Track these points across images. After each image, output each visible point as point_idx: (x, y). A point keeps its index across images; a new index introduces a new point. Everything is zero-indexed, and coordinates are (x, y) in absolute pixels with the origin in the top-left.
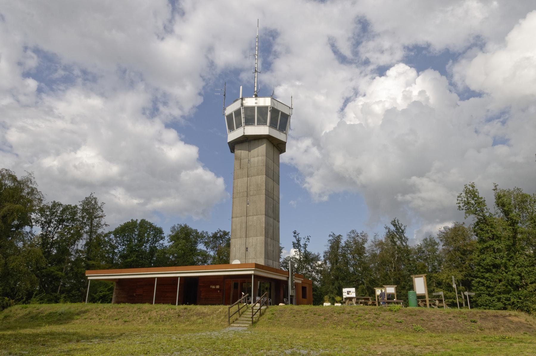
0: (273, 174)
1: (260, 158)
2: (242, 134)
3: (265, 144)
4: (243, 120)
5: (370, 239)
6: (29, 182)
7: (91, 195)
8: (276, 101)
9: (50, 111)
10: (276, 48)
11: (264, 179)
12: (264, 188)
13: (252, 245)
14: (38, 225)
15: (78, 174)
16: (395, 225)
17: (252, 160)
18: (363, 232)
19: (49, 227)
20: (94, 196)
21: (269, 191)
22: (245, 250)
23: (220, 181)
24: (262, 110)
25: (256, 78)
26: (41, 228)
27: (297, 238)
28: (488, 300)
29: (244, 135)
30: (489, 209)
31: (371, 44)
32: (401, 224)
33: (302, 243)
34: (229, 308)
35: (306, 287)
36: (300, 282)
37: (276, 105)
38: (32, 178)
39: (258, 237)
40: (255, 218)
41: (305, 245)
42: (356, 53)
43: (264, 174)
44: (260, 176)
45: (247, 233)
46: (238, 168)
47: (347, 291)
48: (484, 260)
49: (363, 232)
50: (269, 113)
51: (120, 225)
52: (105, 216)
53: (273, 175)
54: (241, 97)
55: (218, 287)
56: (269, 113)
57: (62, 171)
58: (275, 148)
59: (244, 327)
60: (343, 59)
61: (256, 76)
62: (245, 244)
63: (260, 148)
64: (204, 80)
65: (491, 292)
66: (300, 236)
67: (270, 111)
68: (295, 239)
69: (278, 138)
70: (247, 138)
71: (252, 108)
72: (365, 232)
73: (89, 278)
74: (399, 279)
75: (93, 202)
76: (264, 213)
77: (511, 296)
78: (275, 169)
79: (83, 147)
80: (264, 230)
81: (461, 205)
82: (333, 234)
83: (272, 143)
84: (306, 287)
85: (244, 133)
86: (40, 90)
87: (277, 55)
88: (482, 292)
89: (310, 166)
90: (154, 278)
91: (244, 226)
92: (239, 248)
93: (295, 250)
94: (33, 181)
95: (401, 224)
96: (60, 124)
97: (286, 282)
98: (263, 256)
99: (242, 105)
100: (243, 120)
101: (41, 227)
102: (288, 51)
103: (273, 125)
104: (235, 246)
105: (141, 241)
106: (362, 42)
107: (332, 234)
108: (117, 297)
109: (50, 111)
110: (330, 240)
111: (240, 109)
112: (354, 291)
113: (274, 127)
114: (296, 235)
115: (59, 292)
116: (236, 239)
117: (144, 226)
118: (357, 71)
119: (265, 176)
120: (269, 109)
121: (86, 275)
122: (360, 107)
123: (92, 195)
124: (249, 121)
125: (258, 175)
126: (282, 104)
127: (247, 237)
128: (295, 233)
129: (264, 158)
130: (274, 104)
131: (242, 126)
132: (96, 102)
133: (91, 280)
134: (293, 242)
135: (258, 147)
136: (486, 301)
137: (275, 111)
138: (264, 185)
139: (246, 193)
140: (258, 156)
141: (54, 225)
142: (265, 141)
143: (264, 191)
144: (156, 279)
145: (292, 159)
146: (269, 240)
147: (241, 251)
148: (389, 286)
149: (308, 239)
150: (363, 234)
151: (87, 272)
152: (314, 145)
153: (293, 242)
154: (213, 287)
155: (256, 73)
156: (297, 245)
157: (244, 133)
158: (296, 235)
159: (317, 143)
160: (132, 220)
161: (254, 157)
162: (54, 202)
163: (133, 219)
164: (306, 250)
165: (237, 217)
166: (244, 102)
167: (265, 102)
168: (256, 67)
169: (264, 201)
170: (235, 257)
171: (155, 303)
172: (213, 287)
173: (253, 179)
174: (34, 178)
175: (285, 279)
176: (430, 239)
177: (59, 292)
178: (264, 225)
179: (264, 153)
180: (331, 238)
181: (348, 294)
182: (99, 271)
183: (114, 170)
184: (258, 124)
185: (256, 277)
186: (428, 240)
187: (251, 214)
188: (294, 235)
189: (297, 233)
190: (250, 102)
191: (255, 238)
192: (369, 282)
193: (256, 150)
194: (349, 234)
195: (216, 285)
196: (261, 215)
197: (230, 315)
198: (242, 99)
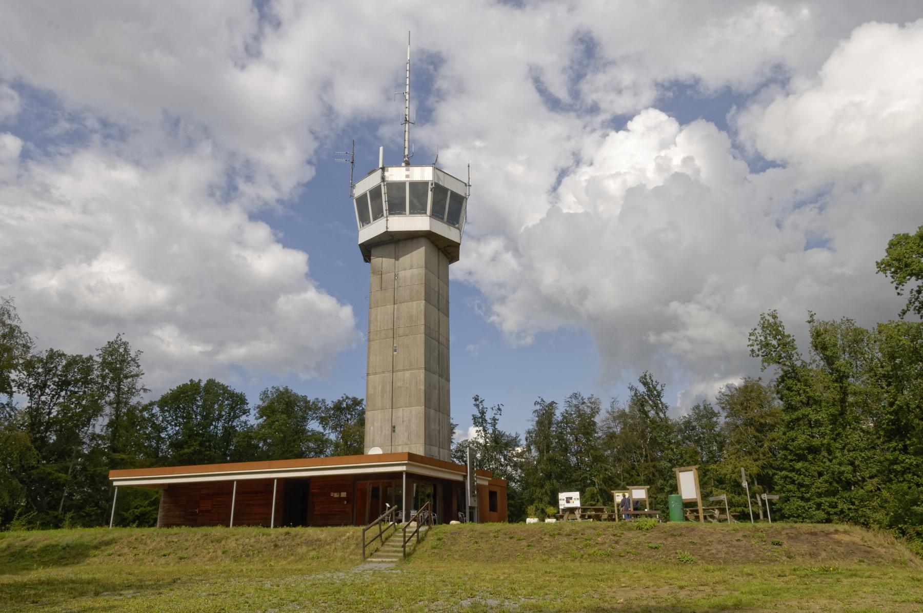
1: (415, 271)
3: (424, 247)
4: (385, 206)
6: (6, 316)
7: (117, 337)
8: (443, 173)
9: (44, 193)
11: (423, 307)
12: (423, 322)
13: (403, 421)
14: (22, 391)
15: (95, 301)
16: (645, 384)
17: (402, 274)
19: (42, 395)
20: (123, 340)
21: (432, 327)
22: (390, 431)
23: (347, 312)
24: (418, 188)
26: (29, 397)
28: (800, 506)
29: (387, 232)
30: (801, 354)
31: (601, 79)
32: (656, 382)
33: (488, 416)
34: (364, 531)
35: (496, 492)
36: (486, 483)
37: (442, 180)
38: (11, 309)
39: (413, 408)
40: (407, 374)
41: (494, 419)
42: (575, 94)
44: (414, 302)
45: (394, 400)
48: (793, 441)
50: (430, 194)
51: (170, 390)
52: (143, 374)
53: (438, 301)
54: (381, 166)
55: (344, 495)
56: (430, 194)
57: (66, 296)
58: (441, 253)
59: (389, 562)
60: (554, 104)
61: (407, 129)
63: (414, 253)
64: (316, 138)
65: (805, 493)
67: (431, 190)
69: (447, 237)
70: (392, 236)
71: (400, 186)
72: (595, 396)
73: (115, 484)
74: (654, 475)
75: (121, 350)
76: (423, 366)
77: (837, 499)
79: (103, 255)
80: (423, 395)
81: (756, 348)
82: (542, 400)
83: (437, 246)
84: (496, 492)
86: (25, 155)
87: (441, 96)
88: (791, 494)
89: (502, 285)
90: (232, 482)
92: (381, 427)
94: (13, 313)
95: (656, 382)
96: (62, 215)
97: (462, 485)
98: (422, 441)
99: (383, 179)
101: (28, 396)
102: (461, 89)
103: (437, 214)
105: (208, 419)
106: (585, 75)
107: (539, 400)
108: (165, 516)
109: (44, 193)
110: (536, 411)
112: (578, 497)
113: (438, 217)
117: (213, 390)
118: (579, 123)
120: (430, 186)
121: (110, 479)
122: (584, 184)
123: (119, 338)
124: (396, 208)
125: (412, 300)
126: (449, 177)
127: (394, 407)
128: (476, 400)
131: (383, 215)
132: (126, 175)
133: (119, 487)
134: (473, 415)
135: (412, 252)
136: (798, 509)
137: (439, 190)
138: (423, 317)
140: (411, 267)
142: (423, 241)
143: (422, 328)
144: (235, 482)
145: (470, 273)
146: (432, 412)
147: (384, 433)
148: (636, 487)
149: (499, 409)
150: (593, 400)
151: (112, 472)
152: (507, 248)
153: (473, 415)
154: (336, 495)
155: (407, 125)
156: (480, 420)
158: (478, 402)
159: (513, 246)
161: (405, 269)
162: (52, 350)
163: (194, 380)
165: (376, 374)
166: (386, 174)
167: (423, 174)
168: (407, 113)
170: (373, 442)
171: (234, 525)
172: (336, 495)
173: (404, 307)
174: (15, 308)
175: (460, 479)
176: (705, 407)
178: (423, 387)
179: (423, 263)
180: (538, 407)
182: (267, 463)
183: (160, 294)
185: (410, 475)
186: (702, 408)
188: (475, 403)
189: (480, 400)
190: (397, 174)
191: (408, 409)
192: (603, 481)
194: (569, 400)
196: (418, 369)
197: (366, 543)
198: (383, 169)
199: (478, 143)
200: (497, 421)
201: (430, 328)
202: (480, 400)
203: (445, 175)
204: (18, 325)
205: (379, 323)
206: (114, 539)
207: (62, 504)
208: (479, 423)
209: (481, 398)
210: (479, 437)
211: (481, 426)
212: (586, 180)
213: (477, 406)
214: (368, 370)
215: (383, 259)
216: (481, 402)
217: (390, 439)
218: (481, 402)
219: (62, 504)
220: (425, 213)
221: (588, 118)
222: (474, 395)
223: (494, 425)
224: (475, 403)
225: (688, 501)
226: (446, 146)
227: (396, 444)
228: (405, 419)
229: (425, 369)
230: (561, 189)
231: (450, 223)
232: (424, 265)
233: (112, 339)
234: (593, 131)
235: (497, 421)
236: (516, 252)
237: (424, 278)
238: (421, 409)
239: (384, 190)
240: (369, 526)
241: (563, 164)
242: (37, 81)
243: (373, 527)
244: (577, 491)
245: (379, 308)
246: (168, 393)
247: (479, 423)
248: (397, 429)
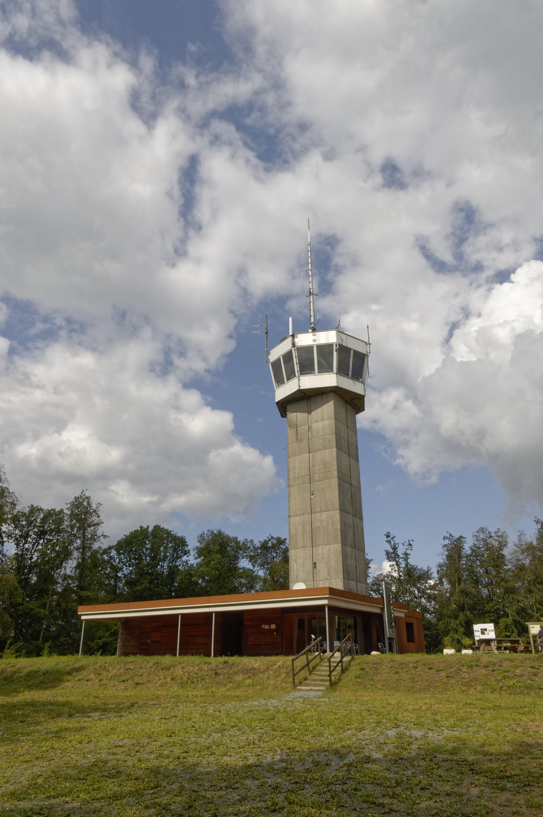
0: (348, 445)
1: (326, 422)
2: (295, 389)
3: (333, 401)
4: (297, 368)
5: (512, 540)
7: (82, 493)
8: (345, 335)
10: (337, 260)
11: (334, 454)
12: (336, 468)
13: (323, 558)
14: (11, 541)
17: (314, 426)
18: (499, 529)
20: (86, 495)
21: (344, 472)
22: (312, 567)
23: (268, 462)
25: (312, 304)
26: (16, 546)
27: (392, 544)
31: (482, 240)
33: (400, 551)
36: (403, 615)
39: (332, 546)
40: (324, 515)
41: (406, 554)
42: (459, 256)
43: (335, 446)
44: (328, 451)
45: (314, 539)
46: (295, 440)
47: (481, 629)
49: (499, 529)
50: (335, 354)
52: (102, 523)
55: (273, 626)
56: (335, 354)
57: (43, 461)
58: (348, 405)
61: (311, 300)
62: (311, 557)
63: (324, 406)
64: (235, 316)
66: (397, 540)
67: (336, 351)
68: (389, 546)
70: (304, 393)
71: (309, 349)
72: (502, 530)
73: (83, 618)
75: (85, 504)
76: (338, 507)
78: (350, 438)
79: (70, 426)
80: (339, 533)
82: (450, 535)
85: (299, 387)
86: (12, 352)
89: (405, 431)
91: (308, 528)
93: (391, 563)
96: (39, 395)
98: (341, 576)
99: (294, 344)
100: (297, 368)
101: (15, 544)
103: (342, 371)
104: (296, 561)
106: (467, 239)
107: (448, 535)
111: (291, 351)
112: (493, 628)
114: (389, 539)
115: (41, 639)
116: (298, 550)
118: (465, 281)
119: (335, 449)
120: (335, 348)
122: (474, 335)
123: (83, 494)
125: (325, 448)
126: (351, 338)
127: (314, 545)
128: (388, 536)
129: (333, 422)
130: (342, 340)
133: (86, 620)
134: (386, 551)
135: (322, 405)
137: (343, 350)
138: (335, 463)
139: (308, 477)
140: (323, 419)
141: (33, 540)
142: (331, 396)
143: (336, 473)
145: (375, 421)
146: (349, 549)
147: (306, 568)
149: (410, 545)
150: (500, 534)
152: (407, 397)
153: (386, 551)
154: (267, 627)
155: (311, 297)
157: (299, 387)
158: (389, 539)
160: (141, 527)
162: (32, 506)
163: (143, 526)
164: (408, 563)
165: (296, 516)
166: (296, 340)
168: (311, 287)
169: (337, 488)
170: (297, 578)
171: (180, 654)
172: (267, 627)
173: (318, 455)
177: (41, 639)
178: (339, 527)
180: (447, 542)
181: (483, 633)
184: (319, 372)
185: (333, 609)
187: (319, 510)
188: (387, 539)
189: (391, 536)
191: (326, 547)
192: (516, 613)
193: (319, 410)
194: (477, 534)
195: (270, 624)
197: (295, 672)
198: (293, 336)
199: (374, 307)
200: (408, 556)
201: (342, 472)
203: (348, 336)
204: (7, 486)
205: (297, 470)
207: (42, 635)
212: (475, 331)
214: (289, 513)
215: (298, 413)
217: (311, 574)
219: (42, 635)
220: (332, 371)
221: (473, 276)
226: (346, 312)
227: (318, 579)
228: (324, 556)
229: (340, 510)
230: (453, 341)
231: (355, 378)
232: (334, 417)
233: (78, 495)
234: (479, 286)
235: (408, 556)
236: (416, 400)
237: (334, 428)
238: (338, 547)
239: (294, 354)
240: (298, 656)
241: (453, 318)
242: (20, 294)
243: (301, 657)
245: (296, 457)
246: (122, 538)
248: (317, 565)
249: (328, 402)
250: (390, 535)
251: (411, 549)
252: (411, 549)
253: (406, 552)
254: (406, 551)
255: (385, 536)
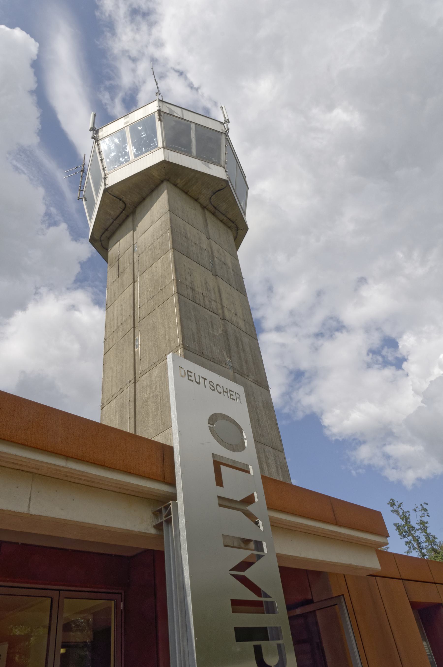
3: (166, 192)
33: (414, 521)
58: (208, 214)
114: (395, 508)
128: (393, 504)
129: (166, 218)
134: (395, 525)
149: (425, 510)
153: (395, 525)
158: (395, 508)
164: (428, 534)
188: (392, 509)
189: (397, 504)
195: (143, 149)
202: (397, 504)
206: (265, 629)
208: (405, 532)
209: (398, 500)
210: (412, 549)
211: (409, 536)
213: (396, 512)
216: (399, 506)
218: (399, 506)
222: (388, 500)
223: (424, 529)
224: (392, 509)
225: (424, 602)
235: (426, 525)
244: (60, 650)
247: (405, 532)
249: (163, 192)
250: (395, 501)
251: (428, 516)
252: (428, 516)
253: (421, 520)
254: (421, 519)
255: (389, 505)
